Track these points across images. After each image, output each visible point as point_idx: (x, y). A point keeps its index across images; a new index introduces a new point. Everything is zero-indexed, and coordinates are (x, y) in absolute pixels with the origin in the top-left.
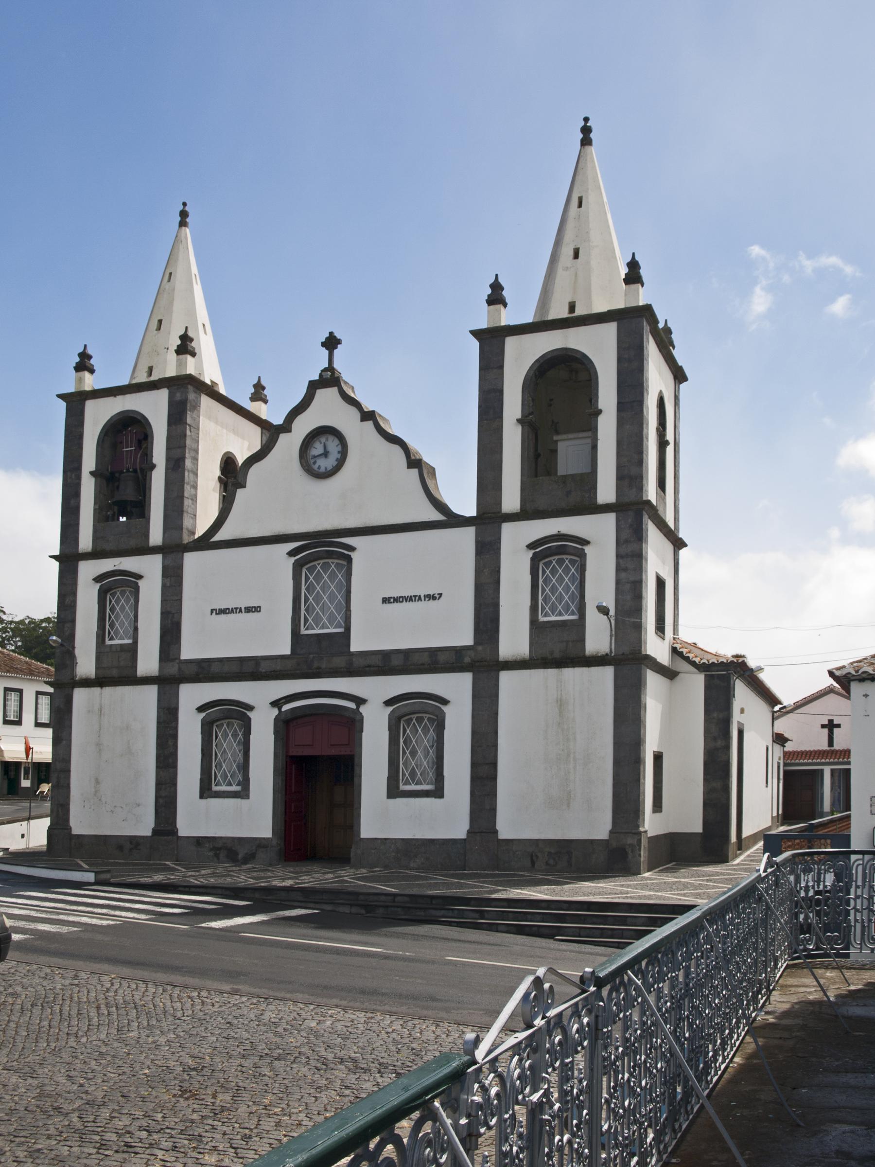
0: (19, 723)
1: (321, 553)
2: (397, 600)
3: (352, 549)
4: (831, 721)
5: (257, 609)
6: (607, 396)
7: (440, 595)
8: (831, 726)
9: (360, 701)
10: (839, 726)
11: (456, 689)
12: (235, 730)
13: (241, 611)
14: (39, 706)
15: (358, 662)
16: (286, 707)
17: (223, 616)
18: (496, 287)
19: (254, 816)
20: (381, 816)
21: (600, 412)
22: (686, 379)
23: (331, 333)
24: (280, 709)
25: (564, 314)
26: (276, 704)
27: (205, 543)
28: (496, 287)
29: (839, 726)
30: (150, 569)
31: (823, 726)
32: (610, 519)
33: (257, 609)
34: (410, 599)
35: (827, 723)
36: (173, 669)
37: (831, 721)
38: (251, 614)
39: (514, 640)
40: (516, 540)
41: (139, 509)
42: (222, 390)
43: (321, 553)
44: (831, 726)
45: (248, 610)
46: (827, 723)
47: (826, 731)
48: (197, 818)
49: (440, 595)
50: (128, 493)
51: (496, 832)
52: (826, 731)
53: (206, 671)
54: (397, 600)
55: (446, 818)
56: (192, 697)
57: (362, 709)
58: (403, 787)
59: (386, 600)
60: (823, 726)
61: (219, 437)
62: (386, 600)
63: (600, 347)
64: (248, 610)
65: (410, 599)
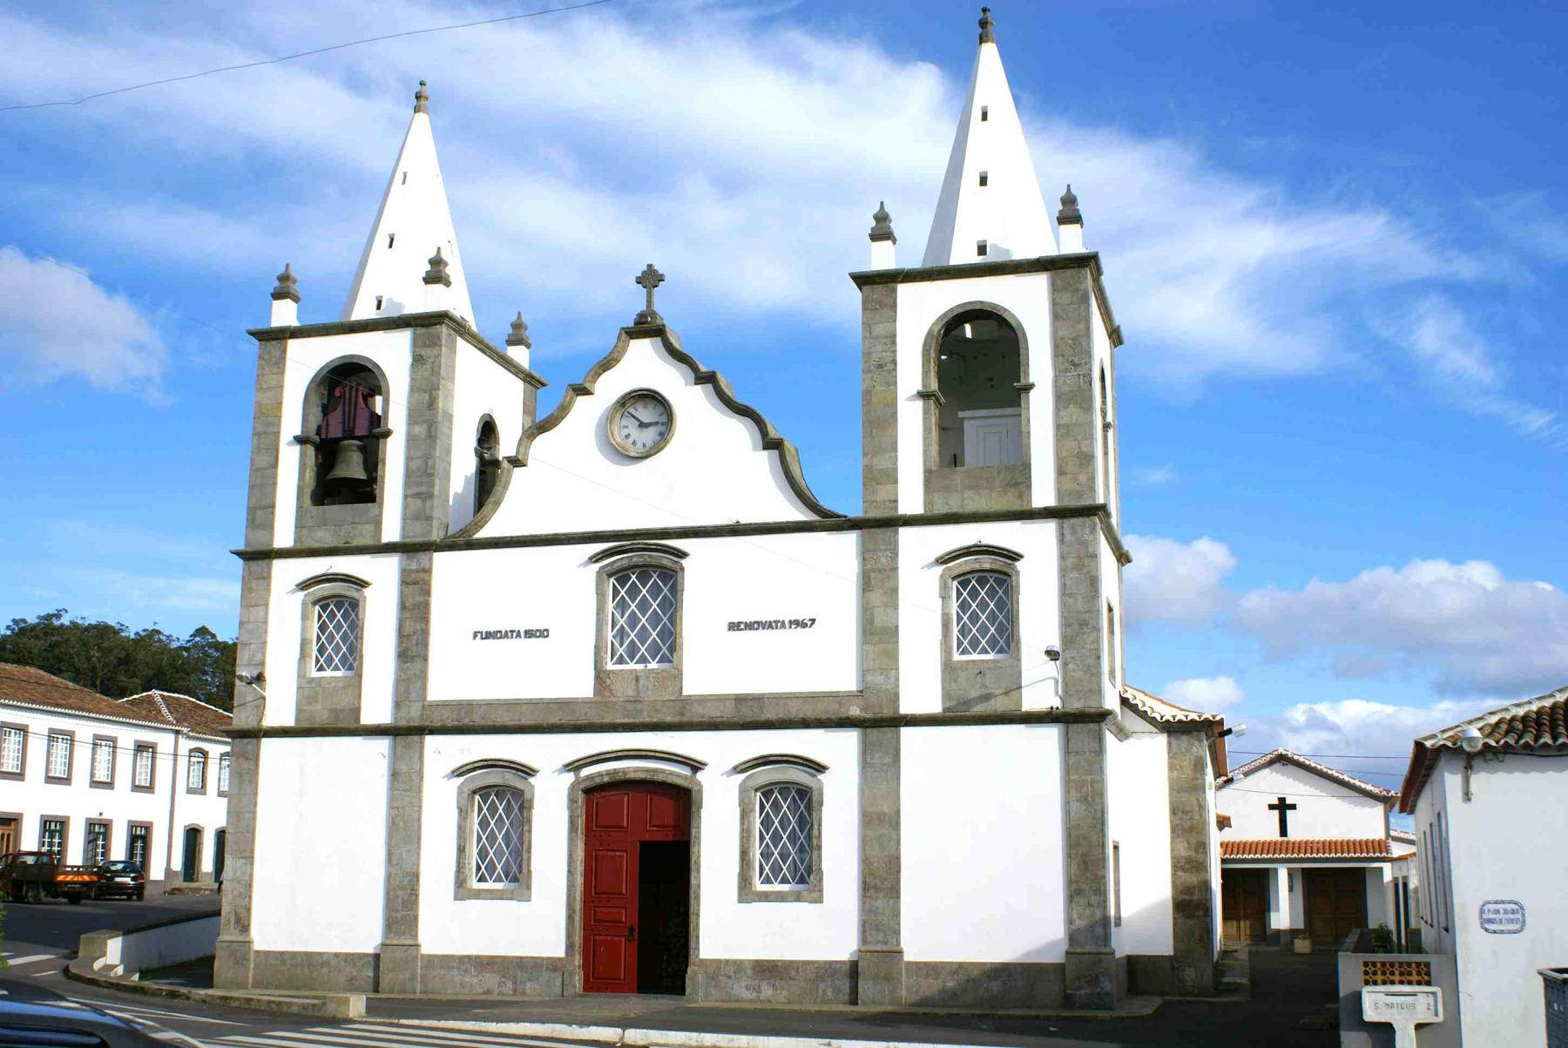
0: (150, 789)
1: (643, 565)
2: (750, 626)
3: (682, 555)
4: (1282, 800)
5: (544, 634)
6: (1040, 366)
7: (813, 621)
8: (1282, 807)
9: (696, 766)
10: (1293, 807)
11: (838, 751)
12: (776, 801)
13: (519, 635)
14: (53, 759)
15: (697, 713)
16: (585, 772)
17: (491, 641)
18: (882, 218)
19: (538, 922)
20: (730, 924)
21: (1031, 386)
22: (1129, 560)
23: (650, 266)
24: (577, 776)
25: (973, 258)
26: (574, 766)
27: (464, 542)
28: (882, 218)
29: (1293, 807)
30: (381, 578)
31: (1272, 807)
32: (1049, 528)
33: (544, 634)
34: (769, 625)
35: (1276, 802)
36: (414, 716)
37: (1282, 800)
38: (533, 640)
39: (920, 689)
40: (920, 552)
41: (365, 491)
42: (473, 325)
43: (643, 565)
44: (1282, 807)
45: (530, 634)
46: (1276, 802)
47: (1276, 812)
48: (454, 927)
49: (813, 621)
50: (352, 468)
51: (900, 952)
52: (1276, 812)
53: (467, 720)
54: (750, 626)
55: (821, 931)
56: (443, 754)
57: (700, 776)
58: (760, 887)
59: (734, 626)
60: (1272, 807)
61: (481, 389)
62: (734, 626)
63: (1027, 302)
64: (530, 634)
65: (769, 625)
